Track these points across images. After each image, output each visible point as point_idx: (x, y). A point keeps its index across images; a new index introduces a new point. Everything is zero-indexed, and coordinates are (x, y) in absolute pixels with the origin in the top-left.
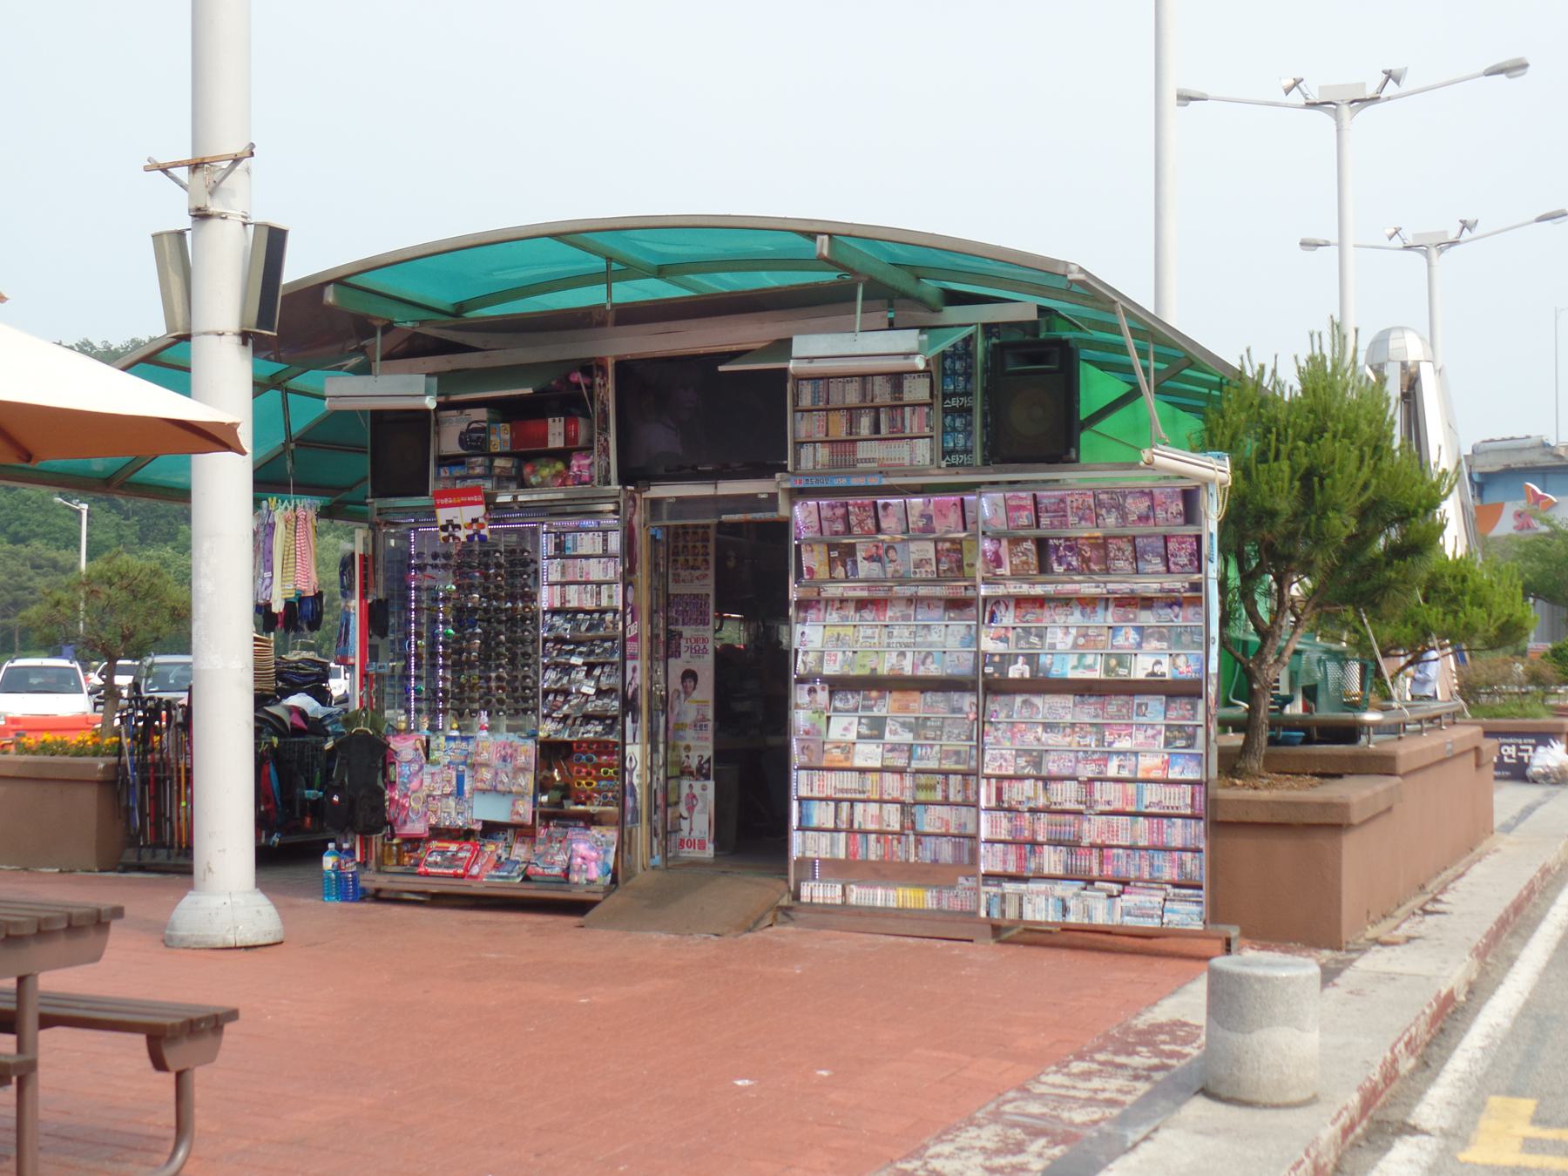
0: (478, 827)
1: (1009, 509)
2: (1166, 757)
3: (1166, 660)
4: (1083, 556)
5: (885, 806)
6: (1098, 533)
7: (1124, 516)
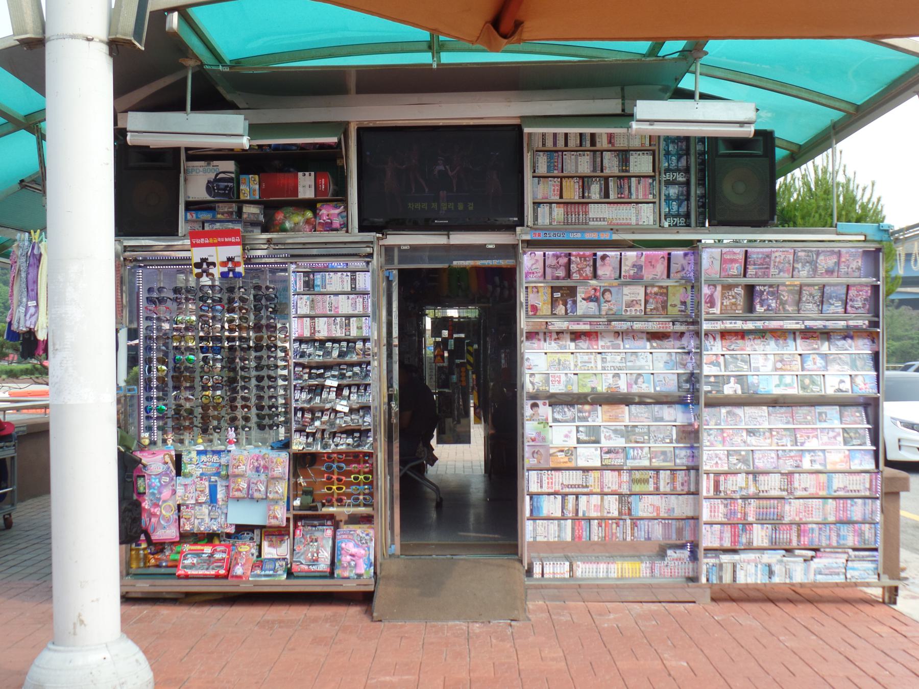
0: (232, 530)
1: (723, 261)
2: (847, 453)
5: (605, 497)
7: (815, 270)
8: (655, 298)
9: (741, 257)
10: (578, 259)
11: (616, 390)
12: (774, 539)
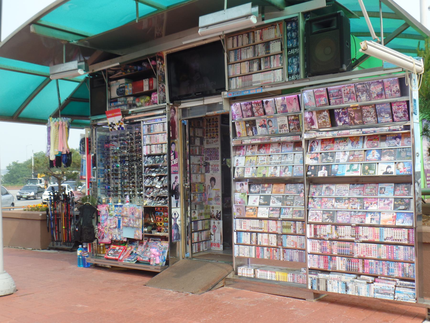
1: (316, 97)
2: (395, 214)
3: (393, 166)
4: (351, 117)
5: (270, 235)
6: (357, 104)
7: (370, 95)
8: (293, 122)
9: (325, 93)
10: (255, 105)
11: (274, 176)
12: (348, 268)
